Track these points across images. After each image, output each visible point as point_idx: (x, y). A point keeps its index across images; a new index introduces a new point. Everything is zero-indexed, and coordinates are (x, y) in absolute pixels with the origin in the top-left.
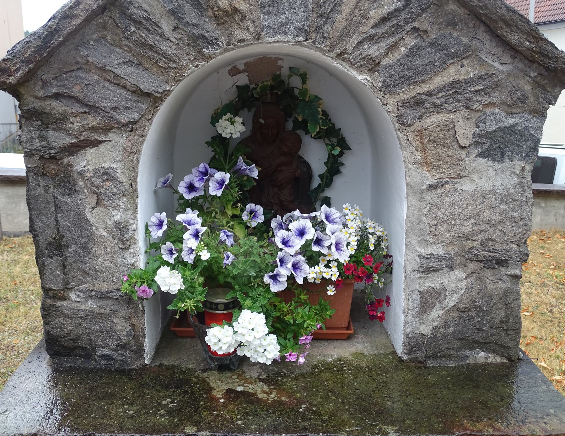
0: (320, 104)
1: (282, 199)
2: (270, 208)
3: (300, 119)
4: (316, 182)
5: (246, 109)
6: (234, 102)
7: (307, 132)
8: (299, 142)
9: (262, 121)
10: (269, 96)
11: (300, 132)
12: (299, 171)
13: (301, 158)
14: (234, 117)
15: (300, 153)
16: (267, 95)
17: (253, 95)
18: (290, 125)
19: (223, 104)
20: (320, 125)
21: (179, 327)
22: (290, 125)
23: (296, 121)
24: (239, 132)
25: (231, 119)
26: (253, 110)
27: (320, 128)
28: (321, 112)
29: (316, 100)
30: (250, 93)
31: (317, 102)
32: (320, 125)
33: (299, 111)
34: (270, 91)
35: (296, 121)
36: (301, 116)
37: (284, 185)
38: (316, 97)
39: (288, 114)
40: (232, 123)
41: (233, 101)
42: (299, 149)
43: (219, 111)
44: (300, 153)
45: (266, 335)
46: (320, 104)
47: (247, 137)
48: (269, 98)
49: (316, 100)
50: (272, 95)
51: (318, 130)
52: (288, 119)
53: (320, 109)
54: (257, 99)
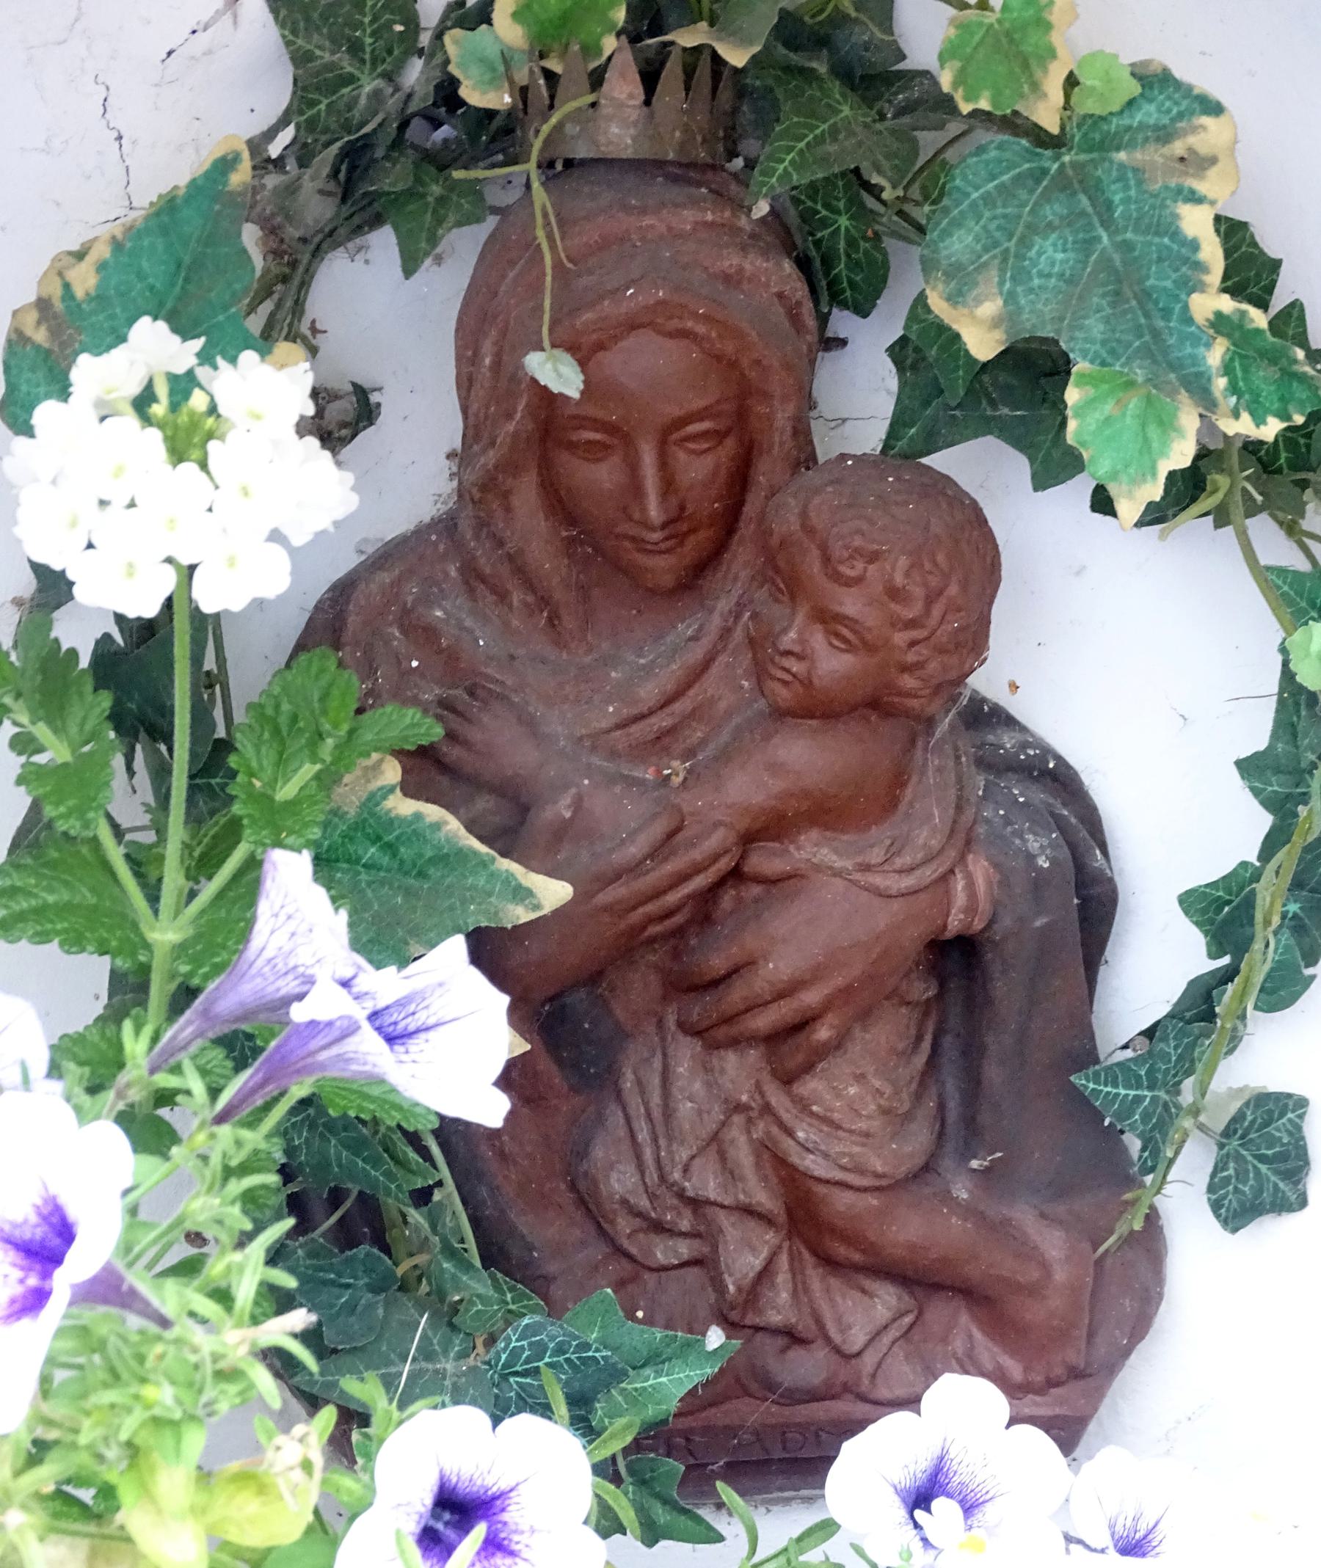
0: (1200, 163)
1: (813, 1164)
2: (685, 1249)
3: (982, 343)
4: (1152, 965)
5: (384, 241)
6: (241, 176)
7: (1054, 465)
8: (971, 560)
9: (557, 373)
10: (624, 87)
11: (983, 468)
12: (979, 867)
13: (985, 716)
14: (206, 357)
15: (987, 681)
16: (597, 79)
17: (447, 93)
18: (859, 395)
19: (147, 194)
20: (1207, 401)
21: (543, 312)
22: (859, 395)
23: (923, 352)
24: (276, 536)
25: (183, 385)
26: (464, 247)
27: (1208, 426)
28: (1212, 253)
29: (1148, 114)
30: (415, 73)
31: (1164, 135)
32: (1207, 401)
33: (959, 245)
34: (633, 35)
35: (923, 352)
36: (990, 308)
37: (823, 1033)
38: (1154, 80)
39: (836, 277)
40: (188, 441)
41: (225, 164)
42: (973, 642)
43: (84, 280)
44: (987, 681)
45: (647, 102)
46: (1200, 163)
47: (420, 532)
48: (619, 120)
49: (1148, 114)
50: (650, 79)
51: (1181, 455)
52: (842, 322)
53: (1196, 223)
54: (496, 135)
